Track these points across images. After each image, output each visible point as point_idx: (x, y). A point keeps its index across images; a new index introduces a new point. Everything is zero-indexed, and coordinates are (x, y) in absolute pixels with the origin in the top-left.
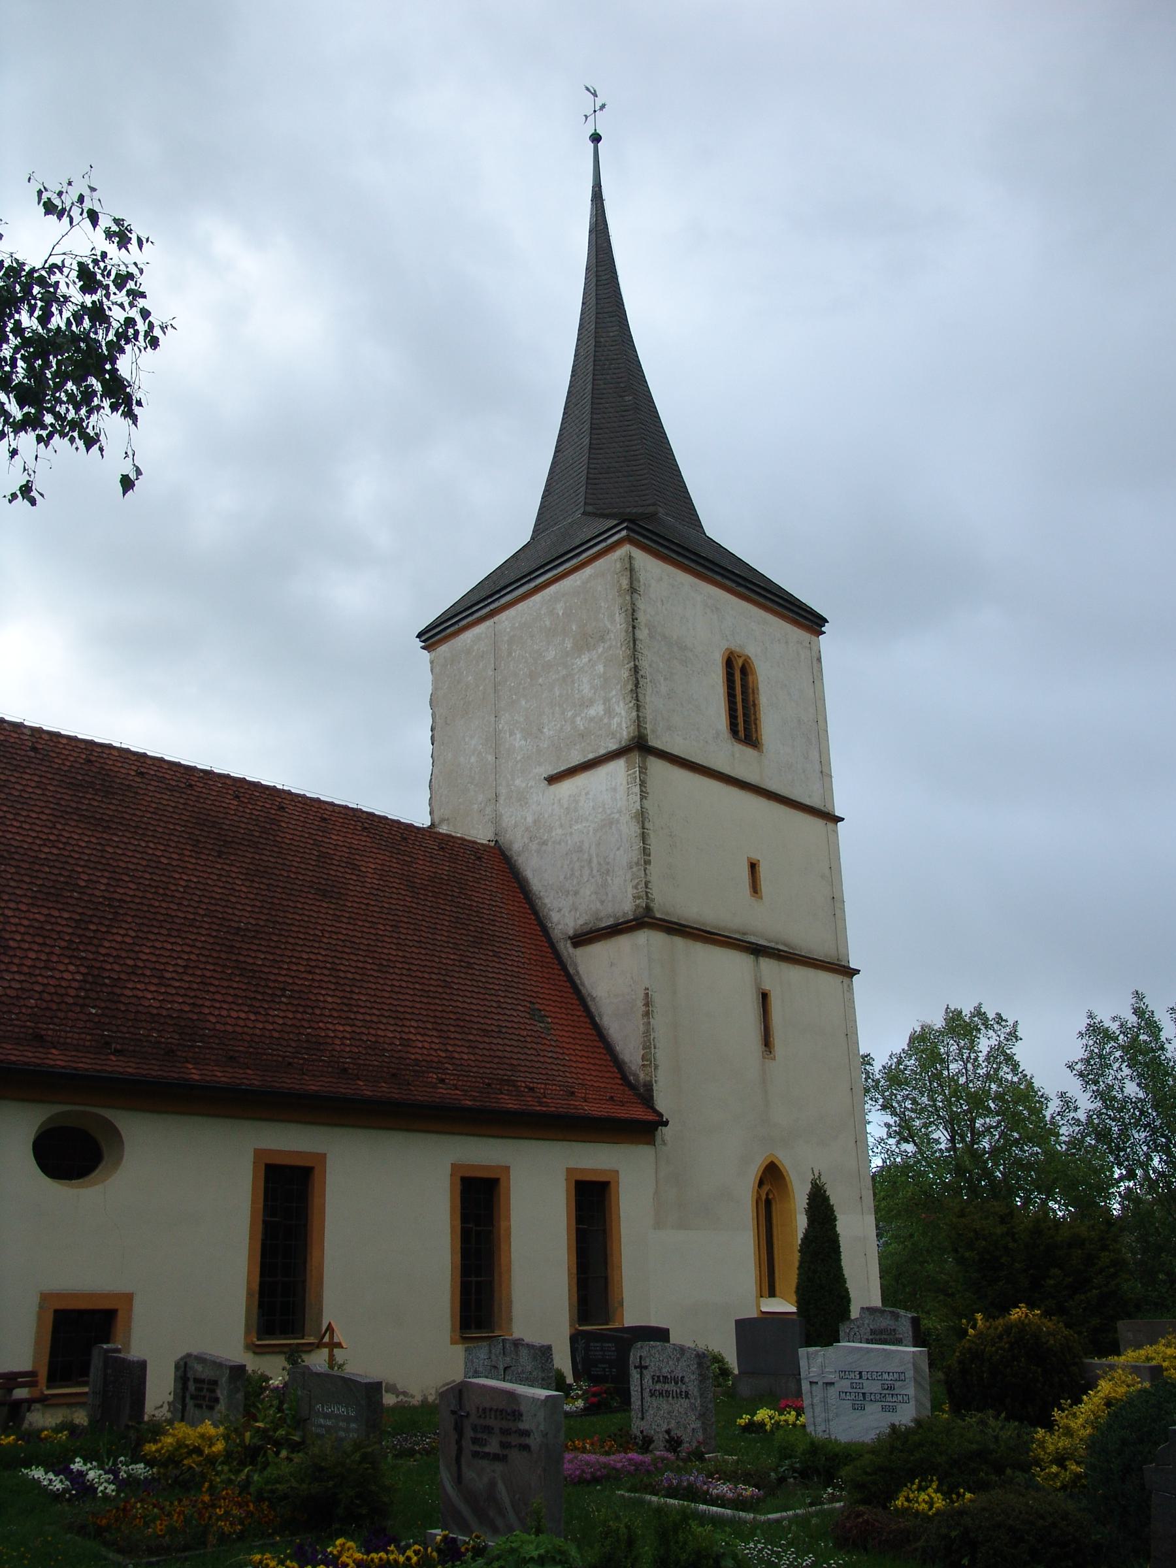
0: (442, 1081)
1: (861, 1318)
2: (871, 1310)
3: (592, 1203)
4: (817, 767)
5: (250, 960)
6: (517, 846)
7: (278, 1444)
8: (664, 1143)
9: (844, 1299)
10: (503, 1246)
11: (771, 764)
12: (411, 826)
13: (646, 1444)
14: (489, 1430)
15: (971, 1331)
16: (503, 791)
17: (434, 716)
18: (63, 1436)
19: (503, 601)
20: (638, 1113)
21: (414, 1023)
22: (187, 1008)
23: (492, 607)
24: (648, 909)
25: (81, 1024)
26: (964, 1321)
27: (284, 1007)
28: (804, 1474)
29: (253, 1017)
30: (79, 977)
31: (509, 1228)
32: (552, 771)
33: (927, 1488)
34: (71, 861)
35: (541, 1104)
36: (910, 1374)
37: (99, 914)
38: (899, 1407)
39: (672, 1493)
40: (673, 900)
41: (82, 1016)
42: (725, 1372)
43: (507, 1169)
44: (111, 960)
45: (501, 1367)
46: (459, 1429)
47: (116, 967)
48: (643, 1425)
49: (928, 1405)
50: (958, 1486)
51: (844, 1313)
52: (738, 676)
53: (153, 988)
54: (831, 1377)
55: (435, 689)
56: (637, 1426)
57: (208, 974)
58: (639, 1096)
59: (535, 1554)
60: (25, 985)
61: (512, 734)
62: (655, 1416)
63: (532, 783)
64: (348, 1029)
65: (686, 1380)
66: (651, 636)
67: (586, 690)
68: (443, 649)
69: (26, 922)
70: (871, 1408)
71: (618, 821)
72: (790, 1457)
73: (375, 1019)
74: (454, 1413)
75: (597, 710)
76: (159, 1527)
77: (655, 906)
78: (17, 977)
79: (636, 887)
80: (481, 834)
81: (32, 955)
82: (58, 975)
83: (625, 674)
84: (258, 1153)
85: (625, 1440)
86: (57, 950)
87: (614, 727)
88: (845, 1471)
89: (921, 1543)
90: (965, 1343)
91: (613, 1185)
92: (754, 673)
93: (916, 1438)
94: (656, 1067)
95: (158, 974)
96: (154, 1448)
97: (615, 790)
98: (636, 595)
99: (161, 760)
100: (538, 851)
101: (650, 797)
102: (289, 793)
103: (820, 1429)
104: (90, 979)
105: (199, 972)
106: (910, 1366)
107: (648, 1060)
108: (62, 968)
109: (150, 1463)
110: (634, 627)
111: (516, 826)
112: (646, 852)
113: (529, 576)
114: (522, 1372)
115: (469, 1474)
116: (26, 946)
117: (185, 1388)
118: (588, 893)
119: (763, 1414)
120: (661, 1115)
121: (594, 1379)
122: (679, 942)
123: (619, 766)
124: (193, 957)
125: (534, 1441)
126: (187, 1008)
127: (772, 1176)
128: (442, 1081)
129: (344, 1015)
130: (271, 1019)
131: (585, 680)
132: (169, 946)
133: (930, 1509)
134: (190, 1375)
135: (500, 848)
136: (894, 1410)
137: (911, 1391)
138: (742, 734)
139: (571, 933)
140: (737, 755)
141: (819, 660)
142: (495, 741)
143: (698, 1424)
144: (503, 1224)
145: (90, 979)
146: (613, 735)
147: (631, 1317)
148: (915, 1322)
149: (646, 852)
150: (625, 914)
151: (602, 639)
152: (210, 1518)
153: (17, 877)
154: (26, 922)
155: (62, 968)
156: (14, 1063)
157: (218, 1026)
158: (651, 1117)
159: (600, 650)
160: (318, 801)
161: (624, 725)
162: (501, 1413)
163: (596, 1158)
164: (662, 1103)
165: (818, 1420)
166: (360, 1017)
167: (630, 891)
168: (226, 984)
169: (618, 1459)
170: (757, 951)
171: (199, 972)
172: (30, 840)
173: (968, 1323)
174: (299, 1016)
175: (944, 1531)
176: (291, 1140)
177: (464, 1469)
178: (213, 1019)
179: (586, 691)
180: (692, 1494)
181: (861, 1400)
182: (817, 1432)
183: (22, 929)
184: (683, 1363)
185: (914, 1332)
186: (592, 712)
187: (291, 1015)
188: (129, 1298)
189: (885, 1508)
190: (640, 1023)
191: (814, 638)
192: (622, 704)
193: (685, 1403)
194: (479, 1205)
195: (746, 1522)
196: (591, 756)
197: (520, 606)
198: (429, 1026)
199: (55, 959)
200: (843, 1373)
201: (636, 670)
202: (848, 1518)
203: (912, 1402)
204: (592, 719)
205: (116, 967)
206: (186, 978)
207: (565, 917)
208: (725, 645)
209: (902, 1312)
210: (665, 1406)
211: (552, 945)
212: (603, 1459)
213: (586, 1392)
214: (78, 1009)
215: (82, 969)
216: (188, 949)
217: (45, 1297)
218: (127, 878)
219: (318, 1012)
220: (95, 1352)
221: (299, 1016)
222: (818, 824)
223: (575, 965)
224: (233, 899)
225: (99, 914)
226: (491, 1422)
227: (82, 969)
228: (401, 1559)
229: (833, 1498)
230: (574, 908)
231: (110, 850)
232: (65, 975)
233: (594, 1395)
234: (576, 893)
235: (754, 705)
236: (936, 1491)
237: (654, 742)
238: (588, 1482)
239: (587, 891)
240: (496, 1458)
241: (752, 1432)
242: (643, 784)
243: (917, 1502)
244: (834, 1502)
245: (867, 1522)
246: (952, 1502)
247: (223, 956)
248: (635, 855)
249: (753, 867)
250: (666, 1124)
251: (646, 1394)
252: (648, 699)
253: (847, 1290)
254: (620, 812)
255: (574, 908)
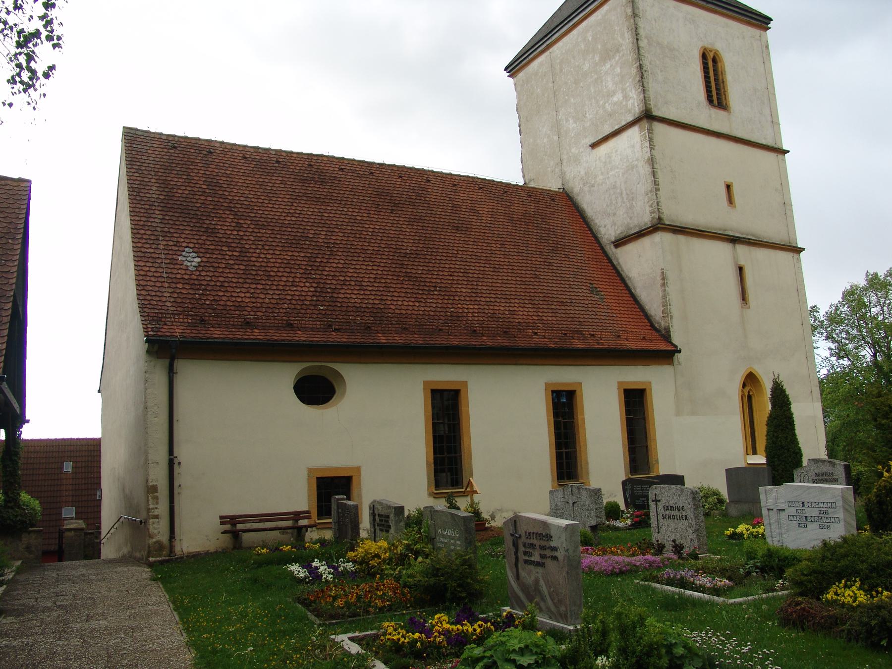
0: (536, 334)
1: (808, 466)
2: (816, 461)
3: (635, 402)
4: (769, 118)
5: (414, 271)
6: (576, 190)
7: (417, 553)
8: (679, 363)
9: (798, 454)
10: (581, 430)
11: (739, 118)
12: (509, 184)
13: (660, 549)
14: (532, 546)
15: (886, 474)
16: (565, 157)
17: (519, 117)
18: (317, 546)
19: (554, 38)
20: (662, 346)
21: (517, 301)
22: (377, 302)
23: (548, 43)
24: (660, 219)
25: (315, 316)
26: (880, 467)
27: (436, 297)
28: (763, 570)
29: (417, 304)
30: (312, 289)
31: (583, 419)
32: (593, 140)
33: (852, 586)
34: (304, 223)
35: (598, 344)
36: (840, 503)
37: (321, 252)
38: (832, 525)
39: (670, 583)
40: (674, 213)
41: (315, 311)
42: (721, 501)
43: (581, 384)
44: (330, 278)
45: (571, 502)
46: (515, 545)
47: (334, 282)
48: (659, 537)
49: (855, 525)
50: (878, 585)
51: (798, 463)
52: (711, 65)
53: (356, 292)
54: (782, 506)
55: (519, 100)
56: (655, 537)
57: (389, 281)
58: (662, 335)
59: (517, 647)
60: (281, 296)
61: (567, 120)
62: (666, 531)
63: (582, 150)
64: (476, 307)
65: (685, 508)
66: (649, 44)
67: (610, 85)
68: (521, 75)
69: (279, 261)
70: (810, 526)
71: (637, 166)
72: (754, 558)
73: (492, 300)
74: (512, 535)
75: (618, 97)
76: (339, 603)
77: (664, 217)
78: (276, 292)
79: (651, 206)
80: (553, 185)
81: (284, 279)
82: (299, 289)
83: (634, 70)
84: (426, 383)
85: (646, 546)
86: (299, 275)
87: (630, 106)
88: (789, 572)
89: (847, 626)
90: (881, 482)
91: (648, 391)
92: (721, 61)
93: (842, 550)
94: (672, 317)
95: (359, 283)
96: (353, 554)
97: (633, 146)
98: (637, 18)
99: (354, 160)
100: (589, 191)
101: (656, 148)
102: (433, 172)
103: (775, 540)
104: (319, 290)
105: (383, 281)
106: (840, 498)
107: (666, 313)
108: (302, 285)
109: (354, 562)
110: (637, 40)
111: (574, 177)
112: (656, 183)
113: (568, 19)
114: (584, 505)
115: (523, 574)
116: (280, 274)
117: (374, 520)
118: (621, 213)
119: (742, 528)
120: (676, 347)
121: (637, 507)
122: (682, 238)
123: (635, 131)
124: (379, 272)
125: (560, 554)
126: (377, 302)
127: (751, 379)
128: (536, 334)
129: (473, 299)
130: (428, 305)
131: (609, 79)
132: (364, 267)
133: (854, 602)
134: (376, 512)
135: (566, 193)
136: (828, 528)
137: (841, 515)
138: (716, 102)
139: (613, 240)
140: (713, 116)
141: (767, 47)
142: (557, 128)
143: (694, 536)
144: (580, 417)
145: (319, 290)
146: (630, 111)
147: (664, 468)
148: (847, 469)
149: (656, 183)
150: (646, 224)
151: (618, 51)
152: (371, 597)
153: (273, 236)
154: (279, 261)
155: (302, 285)
156: (276, 340)
157: (397, 311)
158: (670, 348)
159: (617, 58)
160: (451, 174)
161: (636, 104)
162: (539, 535)
163: (636, 375)
164: (676, 339)
165: (774, 534)
166: (483, 299)
167: (648, 209)
168: (399, 286)
169: (638, 560)
170: (734, 240)
171: (383, 281)
172: (278, 214)
173: (883, 468)
174: (446, 301)
175: (865, 619)
176: (446, 375)
177: (520, 571)
178: (393, 307)
179: (610, 86)
180: (683, 584)
181: (804, 521)
182: (773, 542)
183: (278, 265)
184: (683, 498)
185: (846, 474)
186: (615, 99)
187: (440, 301)
188: (358, 469)
189: (818, 599)
190: (660, 290)
191: (762, 32)
192: (633, 91)
193: (686, 523)
194: (564, 407)
195: (718, 604)
196: (617, 127)
197: (565, 39)
198: (527, 302)
199: (297, 280)
200: (791, 503)
201: (641, 67)
202: (789, 605)
203: (842, 523)
204: (615, 104)
205: (334, 282)
206: (376, 285)
207: (608, 231)
208: (700, 45)
209: (837, 462)
210: (673, 525)
211: (602, 249)
212: (627, 560)
213: (632, 515)
214: (312, 308)
215: (314, 285)
216: (376, 268)
217: (310, 471)
218: (337, 230)
219: (457, 298)
220: (333, 500)
221: (446, 301)
222: (771, 156)
223: (617, 259)
224: (402, 237)
225: (321, 252)
226: (534, 541)
227: (314, 285)
228: (470, 630)
229: (783, 588)
230: (614, 224)
231: (326, 215)
232: (304, 289)
233: (637, 516)
234: (615, 214)
235: (723, 82)
236: (859, 589)
237: (656, 113)
238: (617, 575)
239: (621, 212)
240: (538, 564)
241: (735, 539)
242: (651, 140)
243: (843, 596)
244: (782, 591)
245: (803, 609)
246: (872, 597)
247: (398, 270)
248: (649, 185)
249: (728, 187)
250: (680, 351)
251: (660, 517)
252: (650, 85)
253: (800, 449)
254: (637, 160)
255: (614, 224)
